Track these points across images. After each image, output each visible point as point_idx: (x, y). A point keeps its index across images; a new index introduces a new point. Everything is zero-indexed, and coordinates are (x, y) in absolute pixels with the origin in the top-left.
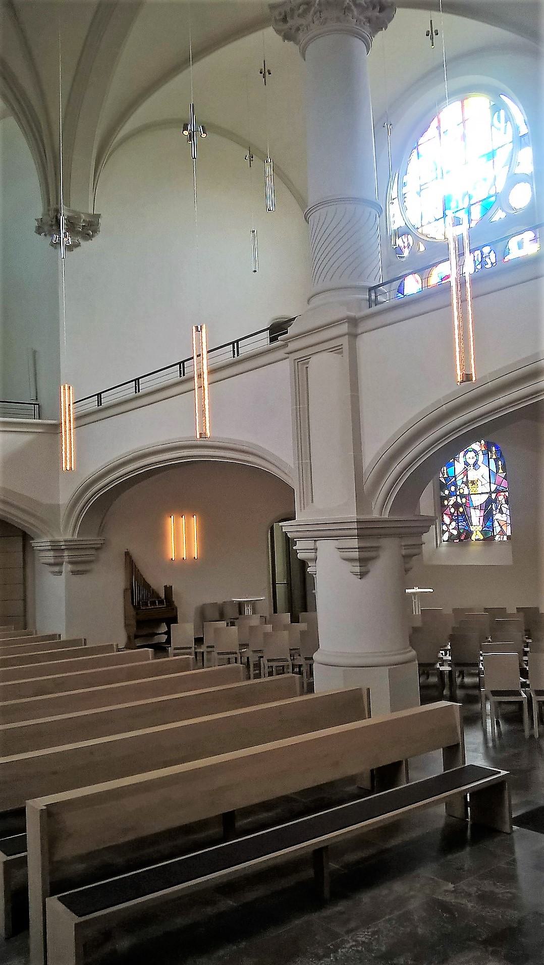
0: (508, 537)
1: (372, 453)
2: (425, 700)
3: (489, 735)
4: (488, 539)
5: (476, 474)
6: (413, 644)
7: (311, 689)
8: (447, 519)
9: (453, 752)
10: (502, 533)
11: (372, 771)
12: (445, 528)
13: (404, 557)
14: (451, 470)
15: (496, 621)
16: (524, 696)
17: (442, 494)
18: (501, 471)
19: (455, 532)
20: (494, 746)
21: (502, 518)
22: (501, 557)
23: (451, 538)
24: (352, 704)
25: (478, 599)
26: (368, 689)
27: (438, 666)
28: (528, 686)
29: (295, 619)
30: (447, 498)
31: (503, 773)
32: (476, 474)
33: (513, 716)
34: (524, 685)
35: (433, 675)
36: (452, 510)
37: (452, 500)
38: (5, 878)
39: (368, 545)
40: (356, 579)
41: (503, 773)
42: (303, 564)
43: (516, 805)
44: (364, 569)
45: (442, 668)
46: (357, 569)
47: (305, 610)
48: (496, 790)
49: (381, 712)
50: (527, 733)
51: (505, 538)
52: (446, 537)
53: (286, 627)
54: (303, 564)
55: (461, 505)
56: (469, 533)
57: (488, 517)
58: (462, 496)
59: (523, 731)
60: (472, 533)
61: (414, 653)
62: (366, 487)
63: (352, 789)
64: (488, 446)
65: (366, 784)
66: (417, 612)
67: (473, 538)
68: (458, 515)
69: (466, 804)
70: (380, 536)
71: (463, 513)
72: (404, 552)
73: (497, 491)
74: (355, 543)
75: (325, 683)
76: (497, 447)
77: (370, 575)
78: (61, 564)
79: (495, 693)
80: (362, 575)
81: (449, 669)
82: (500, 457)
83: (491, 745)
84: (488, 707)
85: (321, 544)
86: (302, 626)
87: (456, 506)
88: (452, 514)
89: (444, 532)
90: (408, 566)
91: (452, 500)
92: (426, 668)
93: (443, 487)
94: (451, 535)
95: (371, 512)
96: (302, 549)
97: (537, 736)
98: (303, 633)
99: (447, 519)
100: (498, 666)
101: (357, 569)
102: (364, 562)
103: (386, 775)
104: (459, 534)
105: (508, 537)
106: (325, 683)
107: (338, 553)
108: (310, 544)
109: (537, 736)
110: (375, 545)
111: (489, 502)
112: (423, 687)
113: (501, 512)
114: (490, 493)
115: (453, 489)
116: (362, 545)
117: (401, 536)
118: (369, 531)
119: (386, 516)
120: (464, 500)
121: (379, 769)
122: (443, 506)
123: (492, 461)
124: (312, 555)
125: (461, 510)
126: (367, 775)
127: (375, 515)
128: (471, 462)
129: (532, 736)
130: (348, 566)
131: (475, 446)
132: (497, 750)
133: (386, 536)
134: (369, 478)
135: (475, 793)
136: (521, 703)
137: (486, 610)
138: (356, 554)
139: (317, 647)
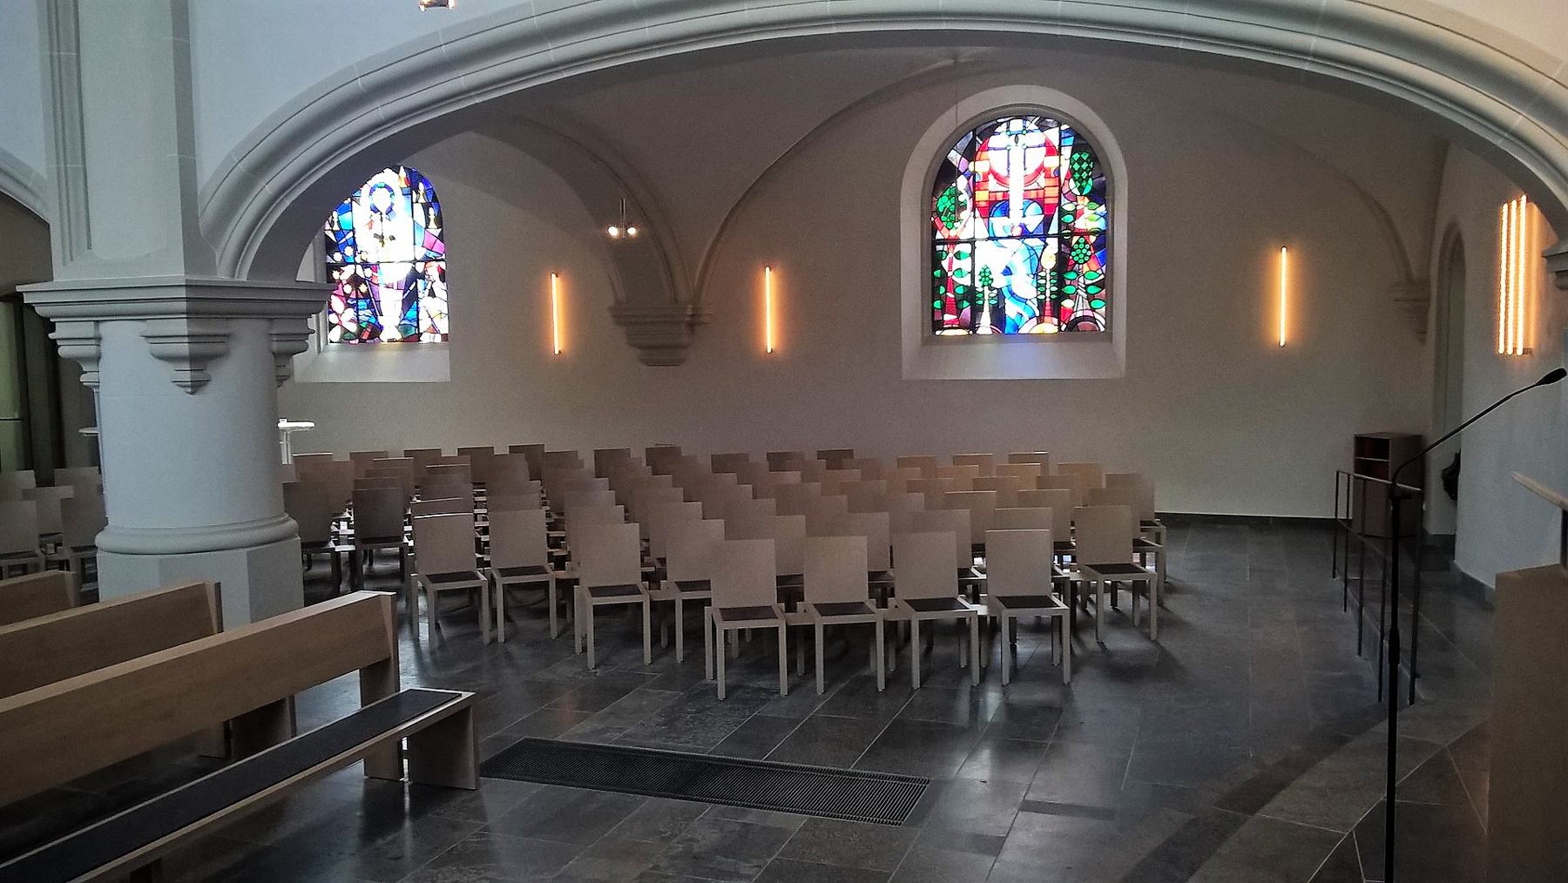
0: (445, 337)
1: (218, 155)
2: (310, 601)
3: (424, 646)
4: (411, 338)
5: (388, 228)
6: (291, 509)
7: (93, 597)
8: (337, 304)
9: (378, 674)
10: (434, 330)
11: (226, 723)
12: (333, 318)
13: (276, 355)
14: (346, 217)
15: (426, 471)
16: (483, 578)
17: (329, 260)
18: (432, 224)
19: (353, 328)
20: (435, 662)
21: (435, 309)
22: (431, 367)
23: (346, 336)
24: (188, 612)
25: (396, 438)
26: (218, 586)
27: (332, 545)
28: (488, 564)
29: (45, 481)
30: (338, 267)
31: (466, 695)
32: (388, 228)
33: (461, 611)
34: (481, 563)
35: (323, 562)
36: (348, 289)
37: (348, 271)
38: (114, 767)
39: (210, 331)
40: (181, 393)
41: (466, 695)
42: (76, 365)
43: (478, 745)
44: (200, 376)
45: (338, 549)
46: (187, 376)
47: (62, 465)
48: (456, 721)
49: (238, 626)
50: (486, 638)
51: (438, 339)
52: (335, 334)
53: (27, 495)
54: (76, 365)
55: (363, 281)
56: (376, 330)
57: (411, 299)
58: (365, 265)
59: (480, 633)
60: (381, 328)
61: (293, 523)
62: (209, 210)
63: (189, 760)
64: (412, 185)
65: (215, 749)
66: (287, 459)
67: (384, 336)
68: (357, 299)
69: (401, 754)
70: (229, 316)
71: (366, 296)
72: (275, 346)
73: (427, 260)
74: (181, 326)
75: (120, 584)
76: (426, 184)
77: (210, 387)
78: (1044, 236)
79: (435, 578)
80: (196, 386)
81: (352, 548)
82: (433, 201)
83: (428, 660)
84: (422, 603)
85: (106, 329)
86: (65, 491)
87: (356, 281)
88: (347, 296)
89: (331, 326)
90: (282, 372)
91: (348, 271)
92: (313, 547)
93: (331, 247)
94: (346, 331)
95: (212, 268)
96: (69, 337)
97: (501, 639)
98: (66, 503)
99: (337, 304)
100: (442, 537)
101: (187, 376)
102: (200, 363)
103: (258, 726)
104: (361, 330)
105: (445, 337)
106: (120, 584)
107: (145, 346)
108: (87, 329)
109: (501, 639)
110: (223, 331)
111: (415, 276)
112: (309, 582)
113: (432, 294)
114: (415, 261)
115: (349, 251)
116: (198, 330)
117: (270, 318)
118: (211, 308)
119: (243, 278)
120: (368, 272)
121: (239, 720)
122: (331, 280)
123: (418, 209)
124: (89, 350)
125: (363, 288)
126: (217, 735)
127: (222, 276)
128: (383, 208)
129: (494, 640)
130: (168, 371)
131: (387, 176)
132: (436, 663)
133: (248, 315)
134: (209, 210)
135: (415, 737)
136: (478, 590)
137: (408, 453)
138: (184, 348)
139: (102, 523)
